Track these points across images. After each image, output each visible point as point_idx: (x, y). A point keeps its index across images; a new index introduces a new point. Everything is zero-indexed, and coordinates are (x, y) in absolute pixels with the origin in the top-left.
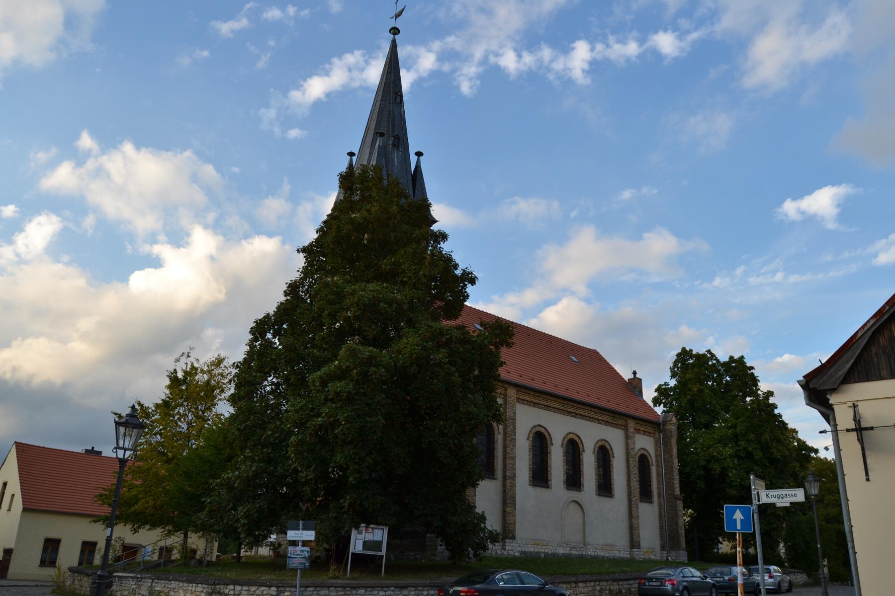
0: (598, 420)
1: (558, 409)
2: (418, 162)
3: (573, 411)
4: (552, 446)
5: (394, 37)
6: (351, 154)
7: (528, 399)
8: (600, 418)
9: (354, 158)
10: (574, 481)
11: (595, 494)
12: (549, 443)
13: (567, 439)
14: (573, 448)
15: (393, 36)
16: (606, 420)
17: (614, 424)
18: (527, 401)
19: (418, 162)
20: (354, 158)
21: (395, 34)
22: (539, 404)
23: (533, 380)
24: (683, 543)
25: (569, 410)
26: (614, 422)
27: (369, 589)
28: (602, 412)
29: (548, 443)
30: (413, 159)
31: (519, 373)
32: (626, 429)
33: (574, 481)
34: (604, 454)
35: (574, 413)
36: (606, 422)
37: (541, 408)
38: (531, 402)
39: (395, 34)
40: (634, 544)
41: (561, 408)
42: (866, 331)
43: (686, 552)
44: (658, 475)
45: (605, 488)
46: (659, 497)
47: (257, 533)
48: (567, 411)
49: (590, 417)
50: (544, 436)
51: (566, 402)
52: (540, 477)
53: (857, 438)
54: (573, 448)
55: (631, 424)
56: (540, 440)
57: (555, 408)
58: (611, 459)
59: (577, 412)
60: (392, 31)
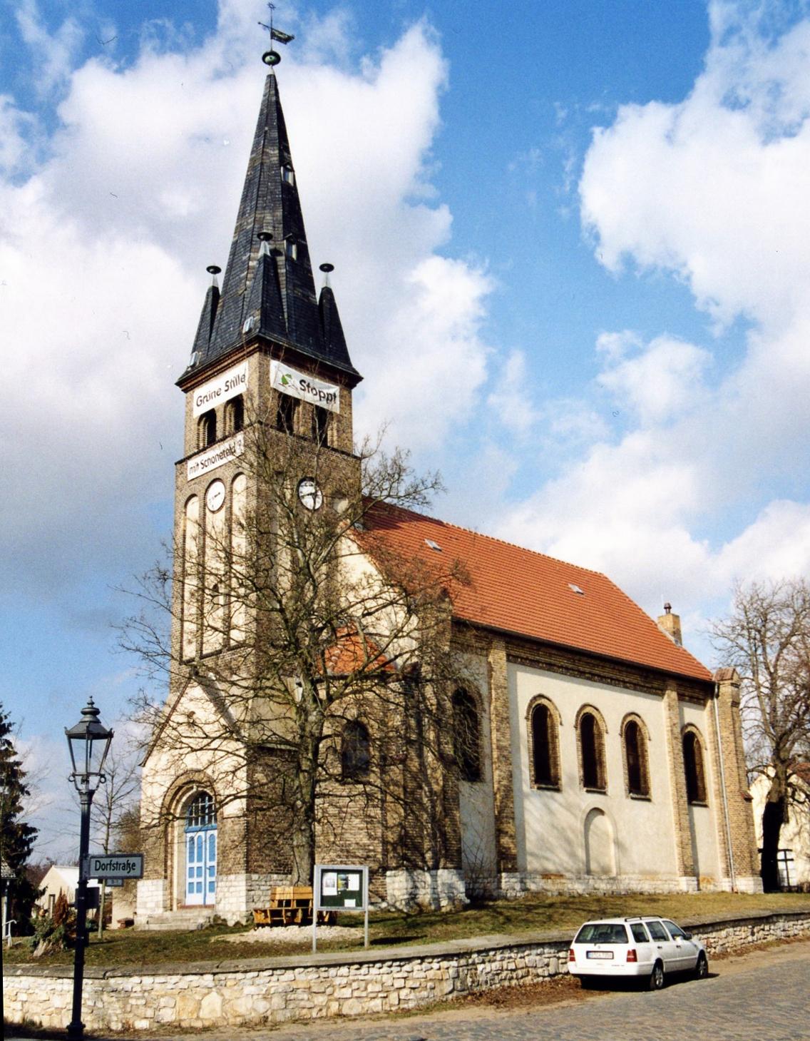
0: (624, 682)
1: (567, 668)
3: (588, 670)
5: (327, 279)
7: (522, 655)
8: (627, 680)
10: (593, 777)
11: (624, 797)
14: (588, 726)
16: (635, 681)
17: (647, 687)
18: (522, 658)
22: (538, 662)
25: (581, 669)
26: (647, 685)
27: (323, 969)
28: (629, 670)
33: (593, 777)
34: (633, 734)
35: (589, 673)
36: (635, 684)
37: (541, 668)
38: (527, 659)
40: (691, 870)
41: (570, 666)
42: (193, 832)
43: (761, 879)
44: (717, 761)
45: (638, 785)
46: (720, 794)
47: (74, 936)
48: (579, 671)
49: (612, 679)
51: (578, 657)
52: (546, 776)
53: (574, 723)
54: (588, 726)
56: (541, 716)
57: (562, 667)
59: (594, 671)
60: (268, 59)
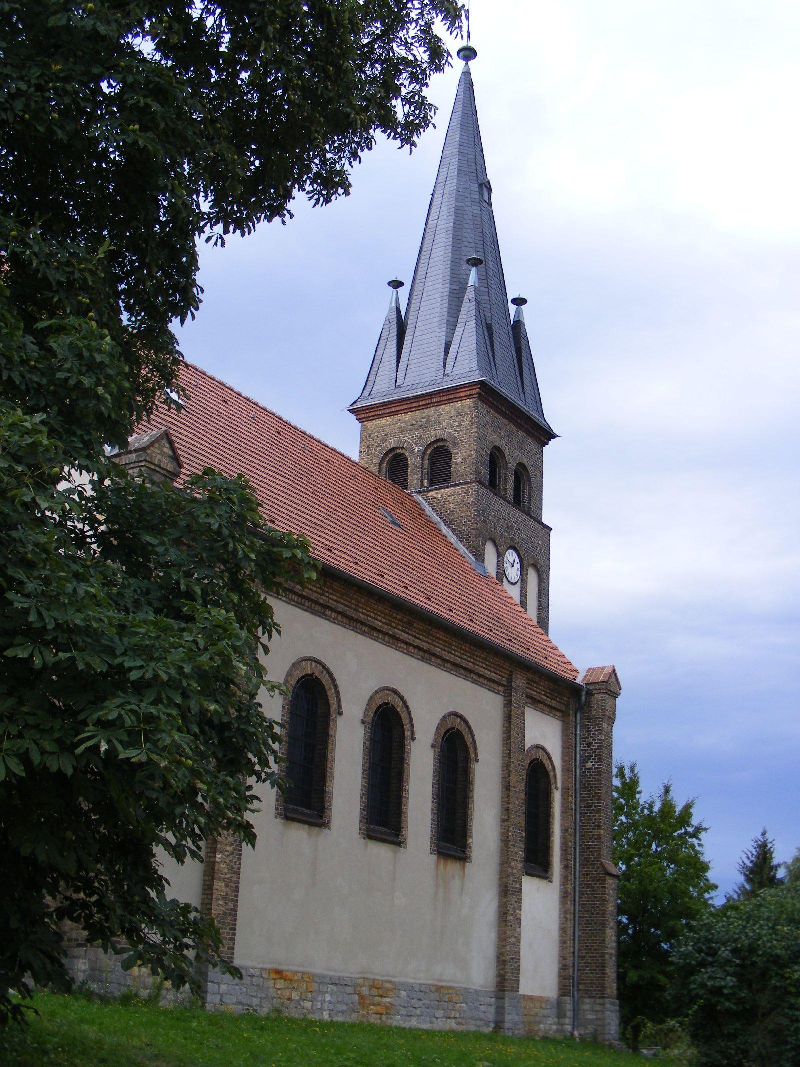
2: (518, 313)
4: (339, 717)
6: (397, 284)
9: (404, 292)
12: (408, 734)
13: (298, 674)
15: (464, 62)
19: (518, 313)
20: (404, 292)
21: (467, 58)
23: (529, 650)
24: (612, 987)
29: (332, 710)
30: (513, 308)
31: (448, 605)
32: (508, 692)
39: (467, 58)
50: (397, 714)
55: (519, 682)
58: (408, 742)
60: (462, 54)
